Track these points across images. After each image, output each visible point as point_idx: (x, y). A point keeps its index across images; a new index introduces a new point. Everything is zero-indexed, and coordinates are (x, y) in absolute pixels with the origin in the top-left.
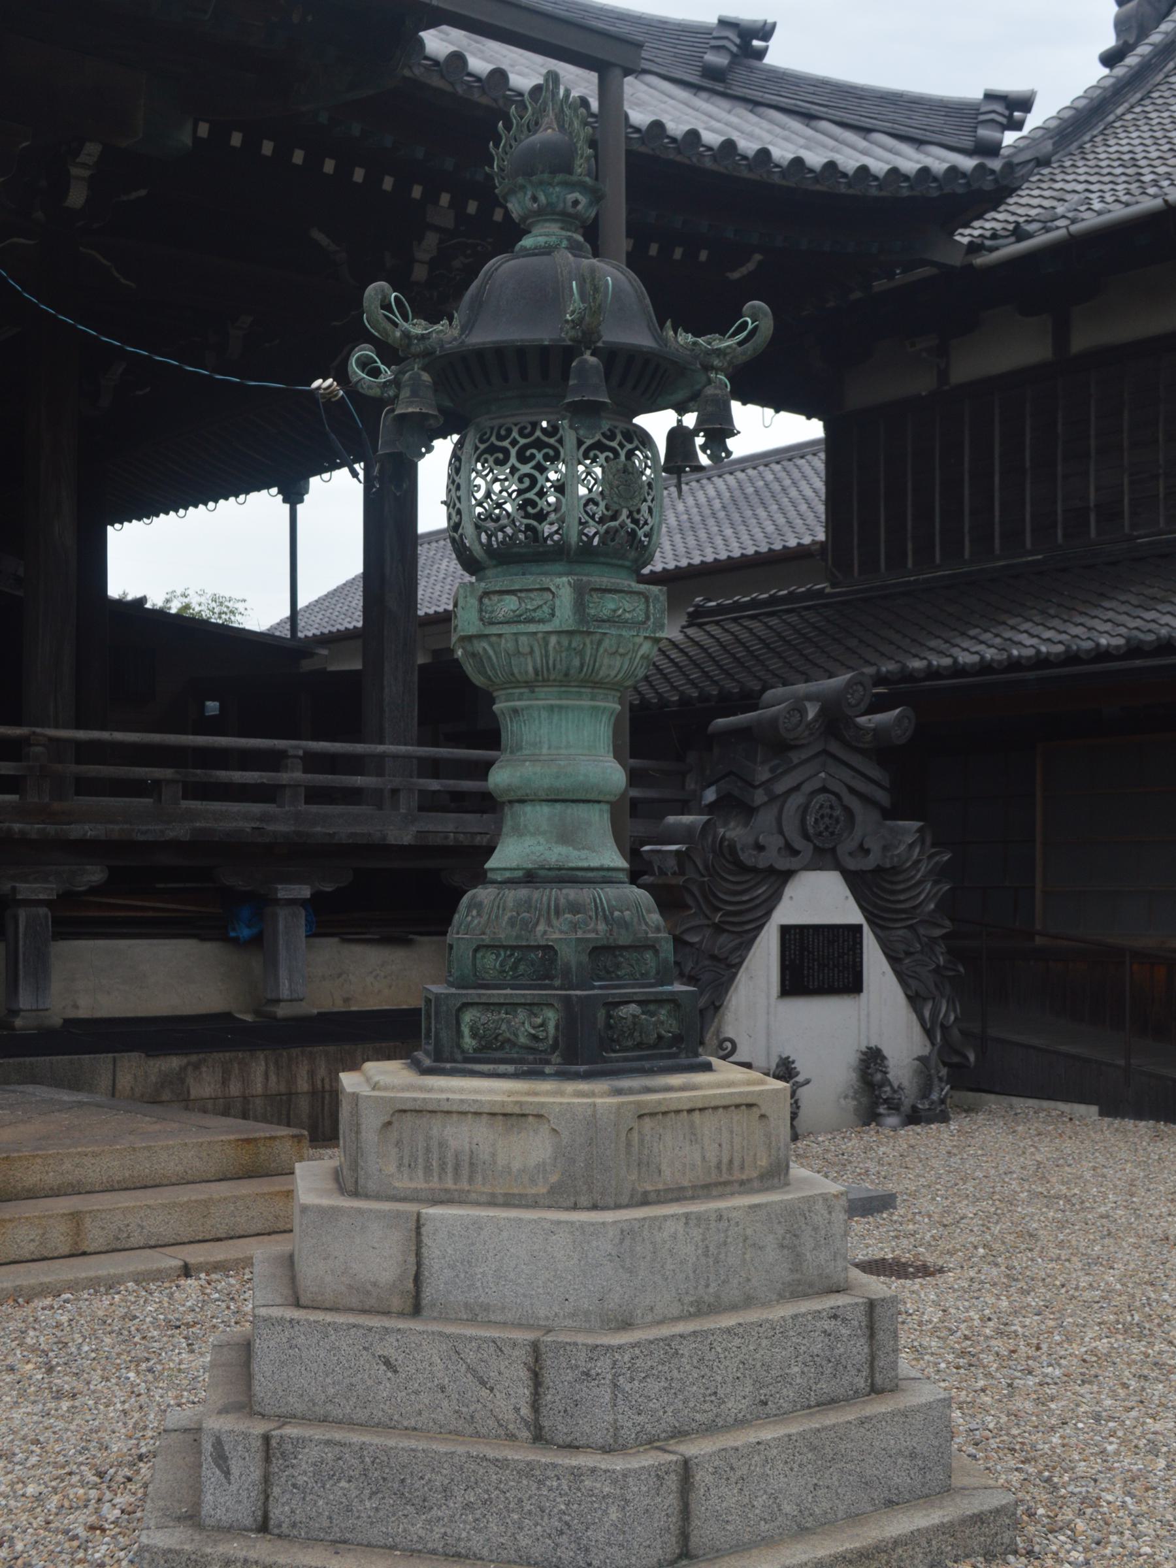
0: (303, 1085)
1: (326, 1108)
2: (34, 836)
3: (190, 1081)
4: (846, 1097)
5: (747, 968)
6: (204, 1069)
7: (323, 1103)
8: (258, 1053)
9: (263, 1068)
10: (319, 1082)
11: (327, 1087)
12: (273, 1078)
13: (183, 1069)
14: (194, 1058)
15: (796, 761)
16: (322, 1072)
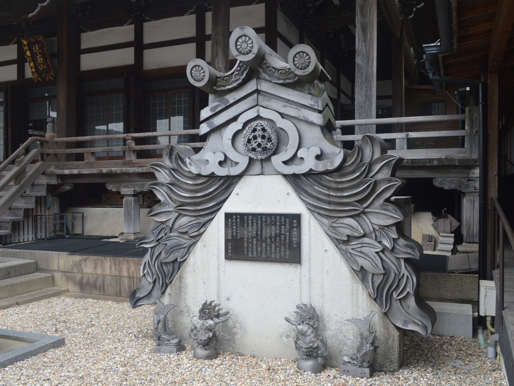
0: (125, 273)
1: (135, 284)
2: (119, 172)
3: (83, 266)
4: (288, 336)
5: (202, 240)
6: (88, 262)
7: (133, 282)
8: (107, 258)
9: (109, 264)
10: (131, 273)
11: (135, 276)
12: (113, 269)
13: (81, 261)
14: (84, 257)
15: (232, 101)
16: (132, 269)
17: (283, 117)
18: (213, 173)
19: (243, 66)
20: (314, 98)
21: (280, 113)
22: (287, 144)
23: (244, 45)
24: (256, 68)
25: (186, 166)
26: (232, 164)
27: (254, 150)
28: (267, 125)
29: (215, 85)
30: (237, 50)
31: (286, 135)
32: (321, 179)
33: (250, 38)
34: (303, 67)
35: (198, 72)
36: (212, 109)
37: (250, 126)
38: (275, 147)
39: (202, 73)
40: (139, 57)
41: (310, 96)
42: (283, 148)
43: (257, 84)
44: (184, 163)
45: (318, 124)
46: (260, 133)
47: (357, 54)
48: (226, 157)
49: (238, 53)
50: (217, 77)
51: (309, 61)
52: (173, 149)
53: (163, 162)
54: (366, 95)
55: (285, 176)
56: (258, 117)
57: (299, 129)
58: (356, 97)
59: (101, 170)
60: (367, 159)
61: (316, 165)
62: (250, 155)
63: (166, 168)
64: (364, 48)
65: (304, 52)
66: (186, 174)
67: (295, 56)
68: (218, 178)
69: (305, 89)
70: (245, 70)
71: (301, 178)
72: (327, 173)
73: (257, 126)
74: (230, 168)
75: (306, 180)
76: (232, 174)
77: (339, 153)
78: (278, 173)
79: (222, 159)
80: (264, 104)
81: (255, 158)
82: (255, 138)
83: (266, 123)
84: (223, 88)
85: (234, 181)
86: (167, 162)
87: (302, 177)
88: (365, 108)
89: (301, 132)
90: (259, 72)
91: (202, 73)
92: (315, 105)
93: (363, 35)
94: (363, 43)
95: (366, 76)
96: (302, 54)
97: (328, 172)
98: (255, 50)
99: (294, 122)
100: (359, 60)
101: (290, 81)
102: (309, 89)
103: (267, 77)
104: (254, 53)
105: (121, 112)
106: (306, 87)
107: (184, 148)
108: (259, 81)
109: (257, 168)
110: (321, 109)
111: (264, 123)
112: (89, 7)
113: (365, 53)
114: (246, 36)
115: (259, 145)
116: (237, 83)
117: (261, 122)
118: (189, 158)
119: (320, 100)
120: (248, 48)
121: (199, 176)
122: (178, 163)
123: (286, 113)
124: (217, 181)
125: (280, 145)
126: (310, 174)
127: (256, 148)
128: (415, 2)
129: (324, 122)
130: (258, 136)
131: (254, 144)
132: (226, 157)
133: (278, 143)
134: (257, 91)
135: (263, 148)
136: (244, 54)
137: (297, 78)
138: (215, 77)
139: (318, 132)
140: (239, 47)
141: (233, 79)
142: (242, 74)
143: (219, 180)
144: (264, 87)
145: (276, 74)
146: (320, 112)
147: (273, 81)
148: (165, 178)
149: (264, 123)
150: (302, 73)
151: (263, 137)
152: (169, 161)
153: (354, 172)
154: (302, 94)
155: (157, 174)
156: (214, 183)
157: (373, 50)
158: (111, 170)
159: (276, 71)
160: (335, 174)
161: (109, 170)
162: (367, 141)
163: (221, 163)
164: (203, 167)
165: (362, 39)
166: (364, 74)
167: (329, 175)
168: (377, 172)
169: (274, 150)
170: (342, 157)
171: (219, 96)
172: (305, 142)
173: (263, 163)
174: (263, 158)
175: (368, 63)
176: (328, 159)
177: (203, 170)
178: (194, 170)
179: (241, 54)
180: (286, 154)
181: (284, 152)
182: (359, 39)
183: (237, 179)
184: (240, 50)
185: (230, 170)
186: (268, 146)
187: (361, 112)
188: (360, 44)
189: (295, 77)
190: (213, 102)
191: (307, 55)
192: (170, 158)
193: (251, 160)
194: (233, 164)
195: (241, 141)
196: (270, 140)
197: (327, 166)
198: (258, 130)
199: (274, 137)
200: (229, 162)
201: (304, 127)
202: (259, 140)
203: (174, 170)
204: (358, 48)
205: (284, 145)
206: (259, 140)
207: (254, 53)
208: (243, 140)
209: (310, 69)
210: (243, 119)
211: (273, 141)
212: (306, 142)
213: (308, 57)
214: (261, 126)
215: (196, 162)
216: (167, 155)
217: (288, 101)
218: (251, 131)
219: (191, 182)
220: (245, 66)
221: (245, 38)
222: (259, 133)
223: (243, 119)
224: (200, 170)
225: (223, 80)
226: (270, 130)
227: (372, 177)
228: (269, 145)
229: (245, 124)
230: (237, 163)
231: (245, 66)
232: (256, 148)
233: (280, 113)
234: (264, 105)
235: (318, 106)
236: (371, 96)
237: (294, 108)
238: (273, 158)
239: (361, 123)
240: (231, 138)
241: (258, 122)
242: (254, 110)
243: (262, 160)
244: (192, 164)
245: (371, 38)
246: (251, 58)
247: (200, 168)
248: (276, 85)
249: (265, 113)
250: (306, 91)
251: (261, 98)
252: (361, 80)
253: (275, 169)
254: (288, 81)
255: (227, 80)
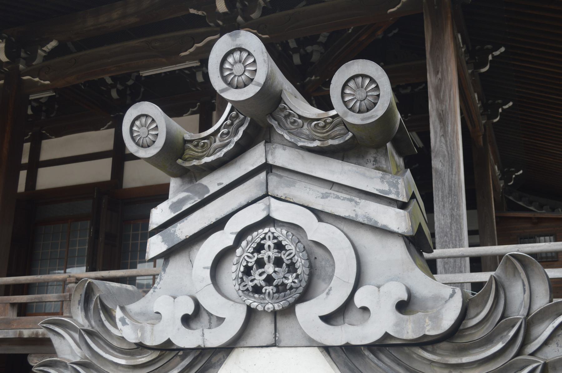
15: (213, 188)
17: (320, 220)
18: (169, 342)
19: (237, 116)
20: (388, 177)
21: (314, 211)
22: (331, 278)
23: (238, 69)
24: (262, 121)
25: (115, 326)
26: (210, 322)
27: (257, 290)
28: (287, 235)
29: (181, 156)
30: (224, 78)
31: (328, 257)
32: (409, 356)
33: (250, 54)
34: (364, 108)
35: (144, 130)
36: (173, 207)
37: (249, 238)
38: (304, 284)
39: (153, 129)
40: (118, 171)
41: (379, 174)
42: (321, 285)
43: (266, 152)
44: (111, 317)
45: (400, 231)
46: (270, 253)
47: (433, 155)
48: (198, 306)
49: (224, 86)
50: (186, 141)
51: (376, 93)
52: (92, 291)
53: (71, 317)
54: (452, 216)
55: (327, 349)
56: (268, 221)
57: (356, 244)
58: (435, 219)
59: (21, 333)
60: (518, 311)
61: (397, 325)
62: (249, 302)
63: (74, 329)
64: (444, 146)
65: (364, 76)
66: (115, 344)
67: (345, 85)
68: (181, 353)
69: (368, 161)
70: (241, 125)
71: (363, 355)
72: (425, 343)
73: (264, 238)
74: (206, 331)
75: (375, 360)
76: (209, 345)
77: (452, 296)
78: (311, 343)
79: (190, 310)
80: (280, 193)
81: (260, 308)
82: (260, 263)
83: (284, 232)
84: (195, 163)
85: (214, 360)
86: (79, 318)
87: (367, 353)
88: (451, 235)
89: (361, 250)
90: (271, 127)
91: (151, 124)
92: (390, 192)
93: (441, 128)
94: (443, 139)
95: (450, 187)
96: (360, 80)
97: (425, 340)
98: (260, 78)
99: (345, 229)
100: (436, 163)
101: (336, 142)
102: (375, 161)
103: (287, 137)
104: (258, 84)
105: (87, 247)
106: (371, 157)
107: (119, 289)
108: (269, 146)
109: (264, 330)
110: (405, 200)
111: (281, 233)
112: (56, 106)
113: (446, 153)
114: (241, 50)
115: (269, 280)
116: (225, 150)
117: (273, 229)
118: (123, 309)
119: (400, 181)
120: (246, 73)
121: (141, 347)
122: (101, 320)
123: (328, 209)
124: (178, 359)
125: (315, 279)
126: (384, 345)
127: (262, 287)
128: (500, 101)
129: (412, 226)
130: (266, 259)
131: (257, 277)
132: (198, 306)
133: (311, 275)
134: (267, 168)
135: (277, 286)
136: (237, 87)
137: (350, 134)
138: (181, 141)
139: (398, 250)
140: (226, 73)
141: (218, 143)
142: (236, 133)
143: (183, 358)
144: (282, 157)
145: (306, 129)
146: (403, 206)
147: (300, 144)
148: (72, 351)
149: (281, 233)
150: (362, 120)
151: (278, 262)
152: (83, 313)
153: (488, 341)
154: (361, 169)
155: (56, 341)
156: (171, 364)
157: (458, 148)
158: (37, 334)
159: (306, 124)
160: (444, 345)
161: (33, 333)
162: (515, 268)
163: (187, 320)
164: (148, 328)
165: (440, 133)
166: (447, 184)
167: (430, 348)
168: (546, 343)
169: (301, 290)
170: (460, 305)
171: (191, 181)
172: (371, 272)
173: (278, 318)
174: (277, 308)
175: (452, 167)
176: (425, 310)
177: (148, 334)
178: (129, 333)
179: (233, 87)
180: (328, 300)
181: (324, 295)
182: (435, 132)
183: (220, 356)
184: (229, 79)
185: (206, 336)
186: (289, 282)
187: (446, 241)
188: (438, 140)
189: (346, 134)
190: (177, 192)
191: (372, 80)
192: (86, 309)
193: (251, 312)
194: (214, 321)
195: (231, 271)
196: (292, 267)
197: (424, 328)
198: (266, 246)
199: (301, 263)
200: (205, 318)
201: (366, 240)
202: (270, 269)
203: (90, 333)
204: (435, 146)
205: (324, 280)
206: (270, 269)
207: (258, 84)
208: (234, 268)
209: (379, 111)
210: (235, 225)
211: (299, 272)
212: (372, 271)
213: (373, 86)
214: (275, 238)
215: (136, 318)
216: (79, 302)
217: (333, 184)
218: (251, 250)
219: (122, 362)
220: (242, 117)
221: (240, 62)
222: (269, 254)
223: (235, 225)
224: (142, 334)
225: (196, 146)
226: (293, 247)
227: (532, 354)
228: (290, 280)
229: (241, 236)
230: (221, 320)
231: (242, 117)
232: (262, 287)
233: (314, 211)
234: (280, 194)
235: (398, 194)
236: (460, 216)
237: (344, 199)
238: (300, 309)
239: (455, 254)
240: (209, 264)
241: (266, 230)
242: (260, 205)
243: (275, 313)
244: (127, 320)
245: (454, 131)
246: (251, 95)
247: (142, 329)
248: (306, 154)
249: (281, 211)
250: (370, 164)
251: (273, 179)
252: (442, 192)
253: (304, 333)
254: (331, 142)
255: (203, 147)
